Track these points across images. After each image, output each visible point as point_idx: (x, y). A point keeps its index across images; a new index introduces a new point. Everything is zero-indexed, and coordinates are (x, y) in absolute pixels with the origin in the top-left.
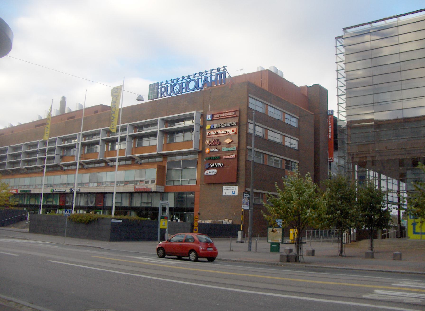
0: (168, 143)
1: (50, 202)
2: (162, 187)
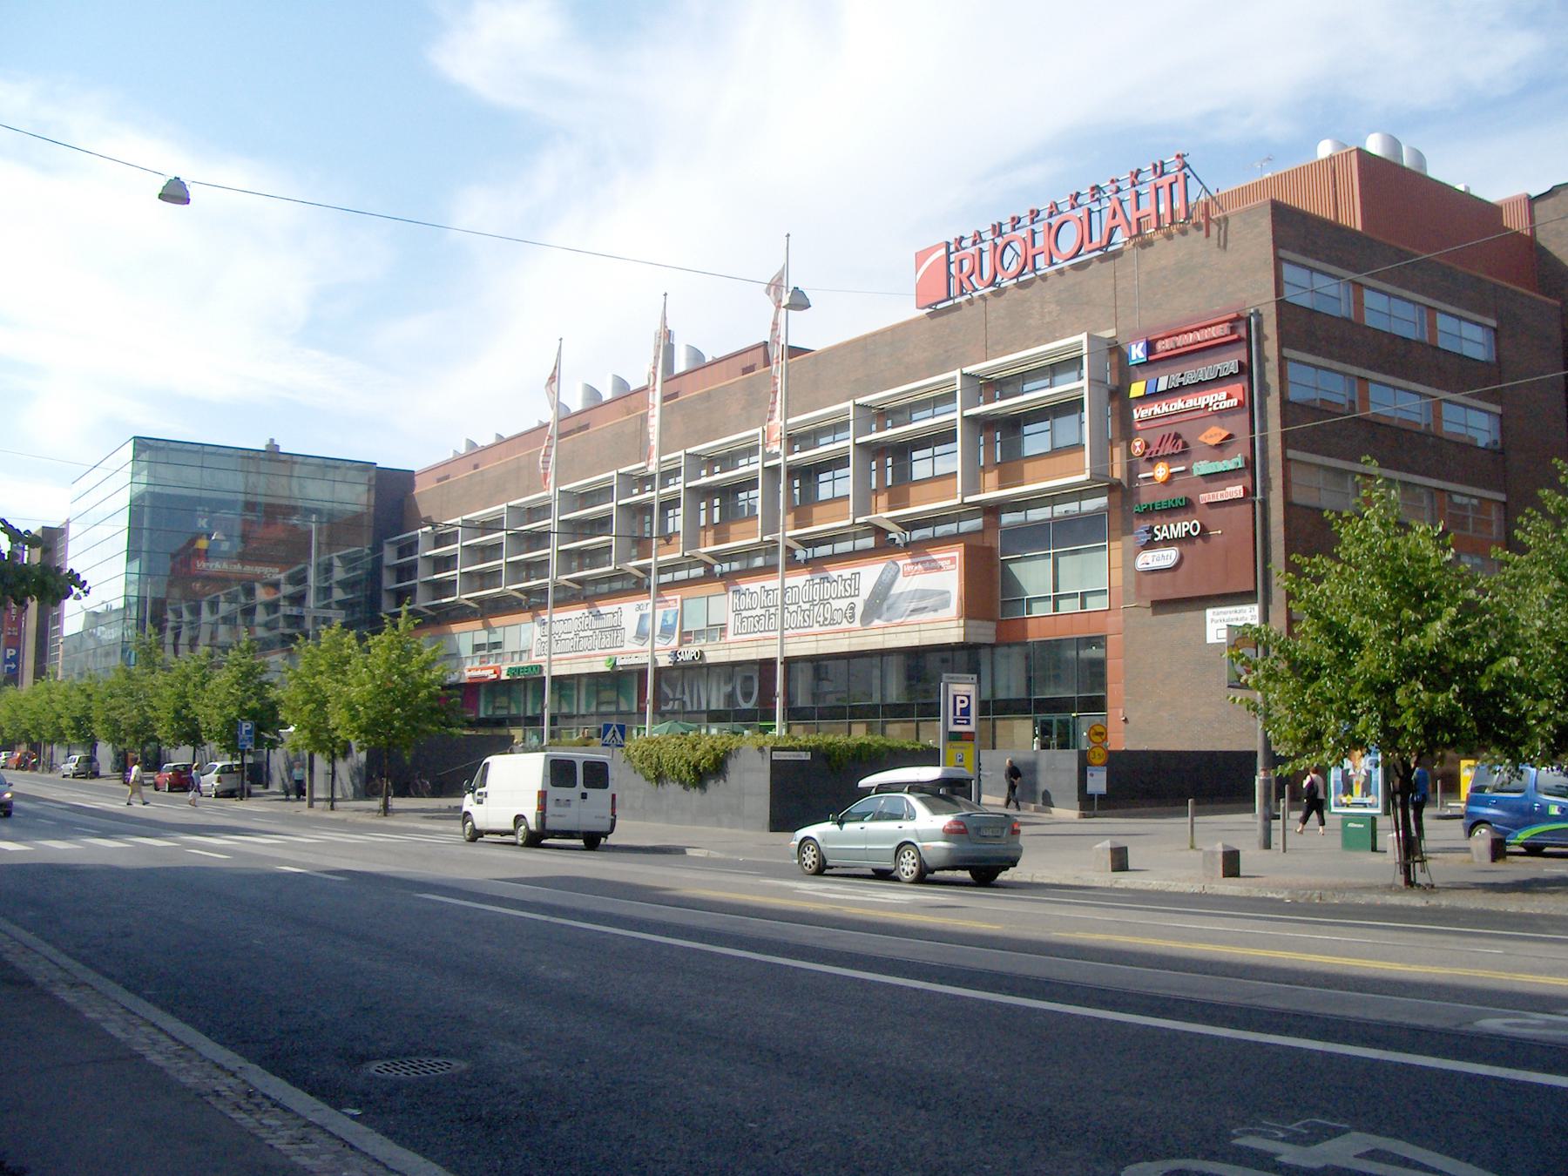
0: (999, 460)
1: (609, 703)
2: (986, 623)
